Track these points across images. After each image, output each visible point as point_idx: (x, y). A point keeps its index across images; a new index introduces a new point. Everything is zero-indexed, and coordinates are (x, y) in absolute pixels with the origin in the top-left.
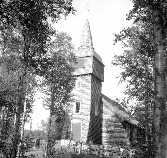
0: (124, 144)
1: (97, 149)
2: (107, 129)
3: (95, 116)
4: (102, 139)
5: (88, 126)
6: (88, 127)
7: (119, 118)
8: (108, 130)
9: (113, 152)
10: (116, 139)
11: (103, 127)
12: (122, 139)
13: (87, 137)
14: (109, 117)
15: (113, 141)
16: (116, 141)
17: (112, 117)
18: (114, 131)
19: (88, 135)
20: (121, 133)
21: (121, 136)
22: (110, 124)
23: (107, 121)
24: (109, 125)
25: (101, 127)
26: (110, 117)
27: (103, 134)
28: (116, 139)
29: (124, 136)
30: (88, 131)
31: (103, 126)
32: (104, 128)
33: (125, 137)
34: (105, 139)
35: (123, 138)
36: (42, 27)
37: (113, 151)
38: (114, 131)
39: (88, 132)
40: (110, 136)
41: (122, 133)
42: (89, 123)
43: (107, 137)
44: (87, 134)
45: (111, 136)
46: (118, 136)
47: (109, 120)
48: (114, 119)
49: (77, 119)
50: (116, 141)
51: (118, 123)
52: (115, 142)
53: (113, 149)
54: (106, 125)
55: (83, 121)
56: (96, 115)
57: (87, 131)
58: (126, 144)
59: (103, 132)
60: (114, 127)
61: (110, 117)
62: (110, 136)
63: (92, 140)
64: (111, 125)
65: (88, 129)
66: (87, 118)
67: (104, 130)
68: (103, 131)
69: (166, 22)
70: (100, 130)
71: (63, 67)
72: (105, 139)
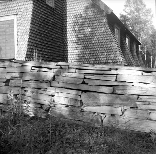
0: (113, 62)
1: (13, 78)
2: (77, 35)
3: (47, 5)
4: (68, 55)
5: (29, 24)
6: (29, 27)
7: (102, 118)
8: (78, 37)
9: (84, 87)
10: (94, 55)
11: (68, 32)
12: (108, 52)
13: (26, 49)
14: (78, 11)
15: (90, 58)
16: (95, 57)
17: (87, 8)
18: (91, 37)
19: (28, 45)
20: (104, 41)
21: (104, 46)
22: (83, 24)
23: (76, 18)
24: (80, 27)
25: (64, 33)
26: (80, 11)
27: (68, 47)
28: (94, 55)
29: (112, 45)
30: (28, 36)
31: (68, 30)
32: (69, 35)
33: (112, 48)
34: (73, 55)
35: (109, 51)
36: (146, 142)
37: (84, 83)
38: (91, 37)
39: (29, 38)
40: (83, 49)
41: (107, 39)
42: (30, 19)
43: (77, 51)
44: (27, 43)
45: (85, 48)
46: (100, 46)
47: (81, 17)
48: (90, 13)
49: (4, 13)
50: (94, 58)
51: (97, 21)
52: (94, 59)
53: (82, 76)
54: (74, 28)
55: (17, 14)
56: (49, 5)
57: (26, 37)
58: (115, 62)
59: (68, 42)
60: (92, 28)
61: (80, 11)
62: (83, 49)
63: (39, 56)
64: (83, 26)
65: (29, 31)
66: (26, 6)
67: (71, 37)
68: (68, 40)
69: (120, 19)
70: (63, 39)
71: (87, 56)
72: (73, 55)
